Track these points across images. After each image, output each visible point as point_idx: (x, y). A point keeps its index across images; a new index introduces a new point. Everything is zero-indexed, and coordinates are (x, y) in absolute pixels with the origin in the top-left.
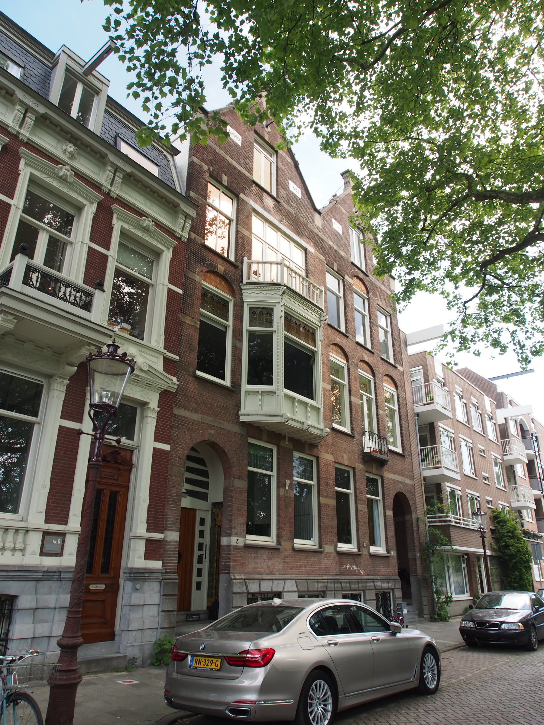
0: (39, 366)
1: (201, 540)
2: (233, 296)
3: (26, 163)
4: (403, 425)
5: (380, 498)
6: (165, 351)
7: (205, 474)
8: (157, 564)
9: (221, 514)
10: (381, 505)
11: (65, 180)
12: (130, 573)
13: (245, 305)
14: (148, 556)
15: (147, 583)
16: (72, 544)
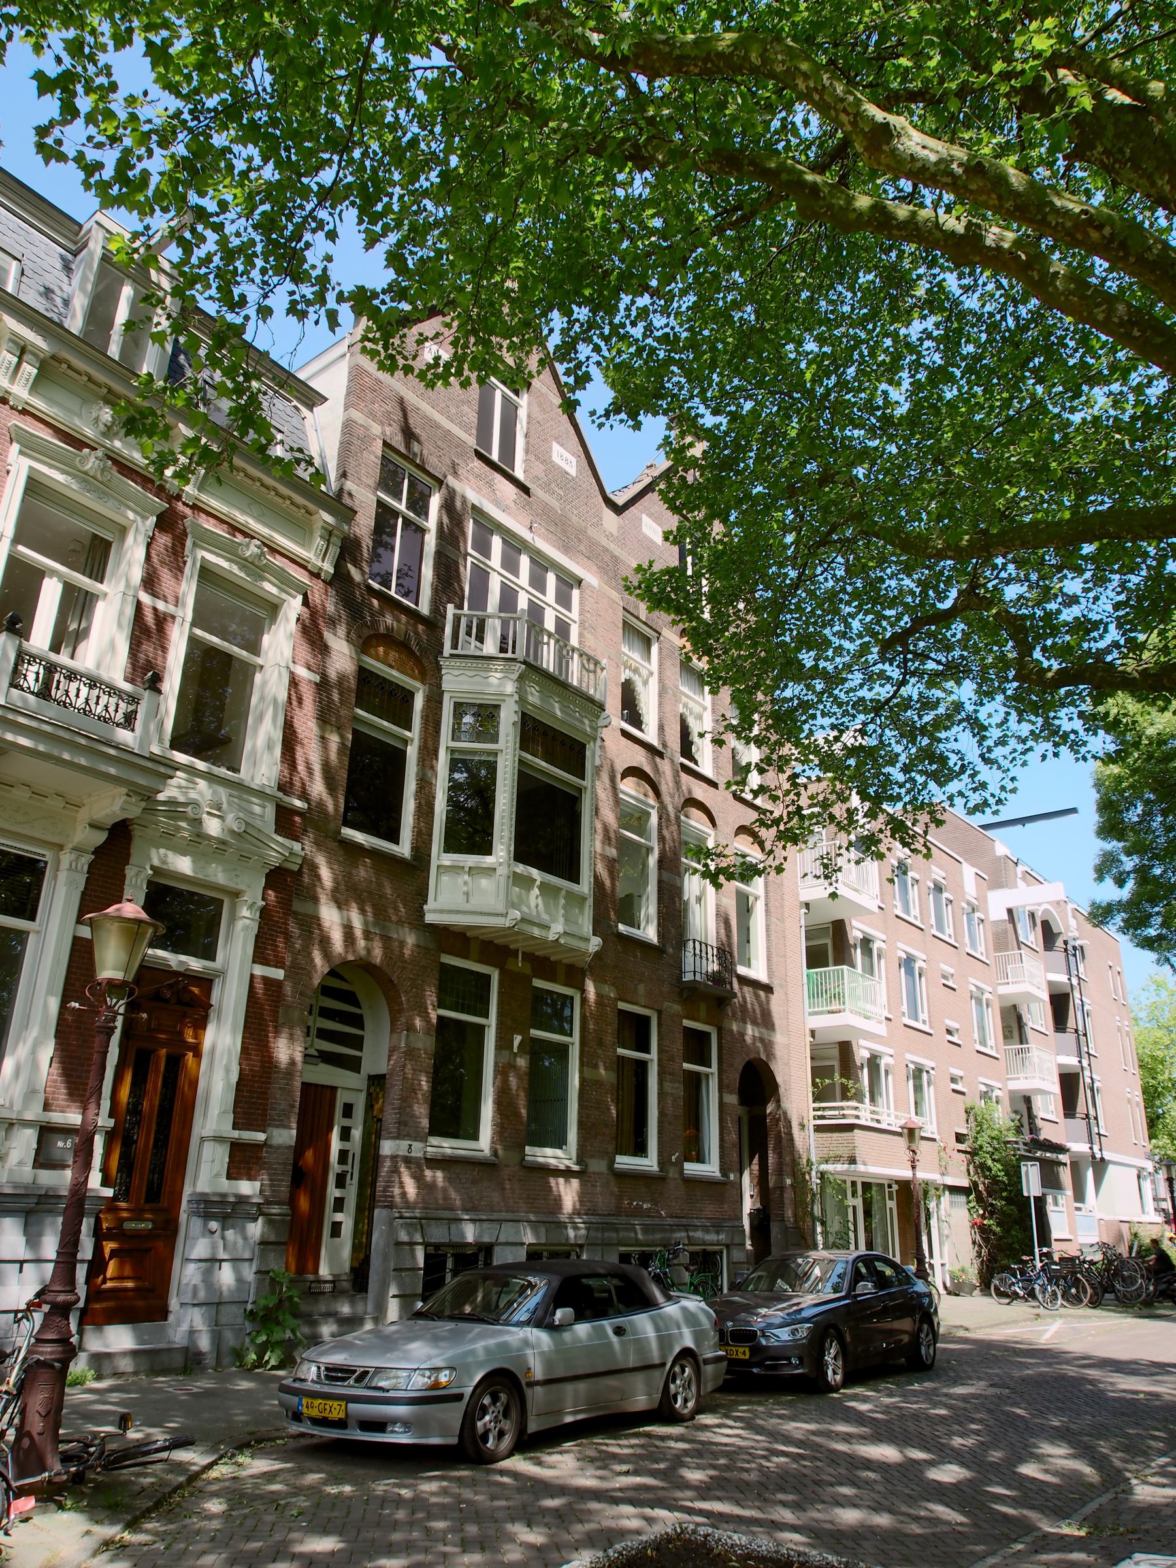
4: (773, 927)
5: (714, 1069)
7: (358, 1021)
10: (714, 1084)
12: (198, 1202)
13: (446, 697)
14: (233, 1173)
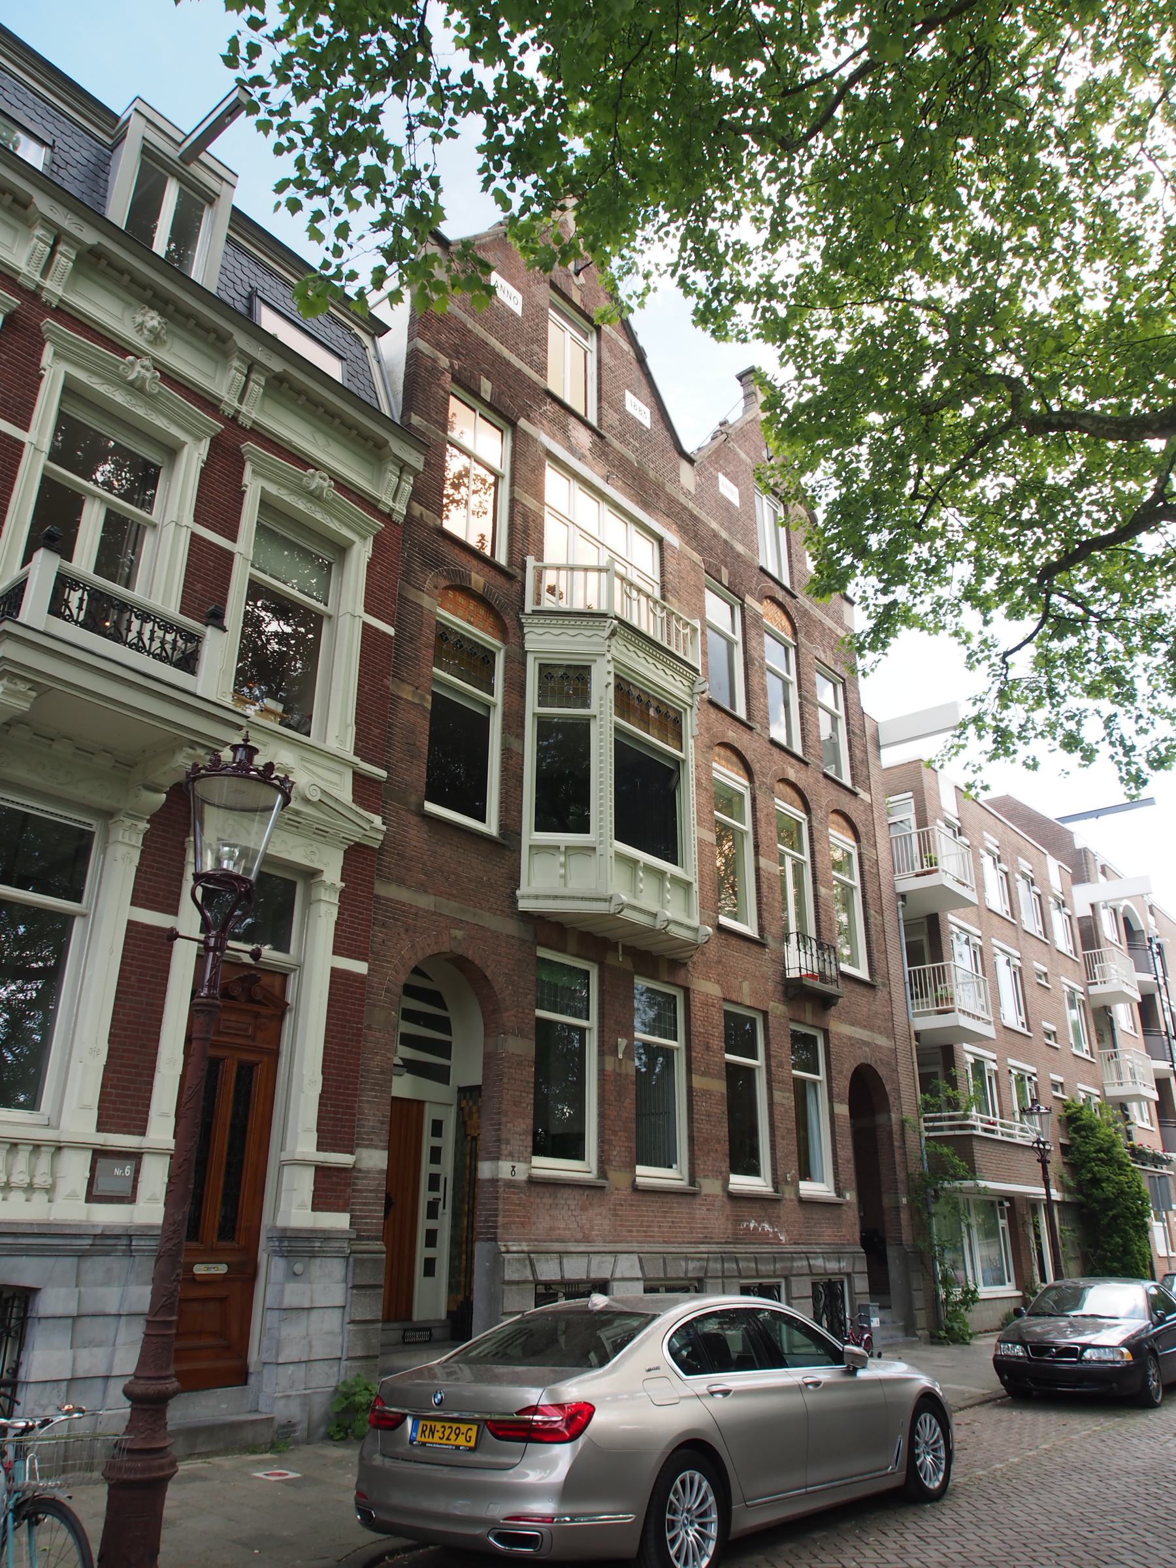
0: (83, 792)
1: (434, 1169)
2: (505, 640)
3: (55, 353)
4: (872, 920)
5: (822, 1077)
6: (357, 760)
7: (444, 1025)
8: (339, 1221)
9: (479, 1111)
10: (823, 1092)
11: (141, 390)
12: (281, 1239)
13: (530, 659)
14: (320, 1202)
15: (318, 1261)
16: (155, 1177)
